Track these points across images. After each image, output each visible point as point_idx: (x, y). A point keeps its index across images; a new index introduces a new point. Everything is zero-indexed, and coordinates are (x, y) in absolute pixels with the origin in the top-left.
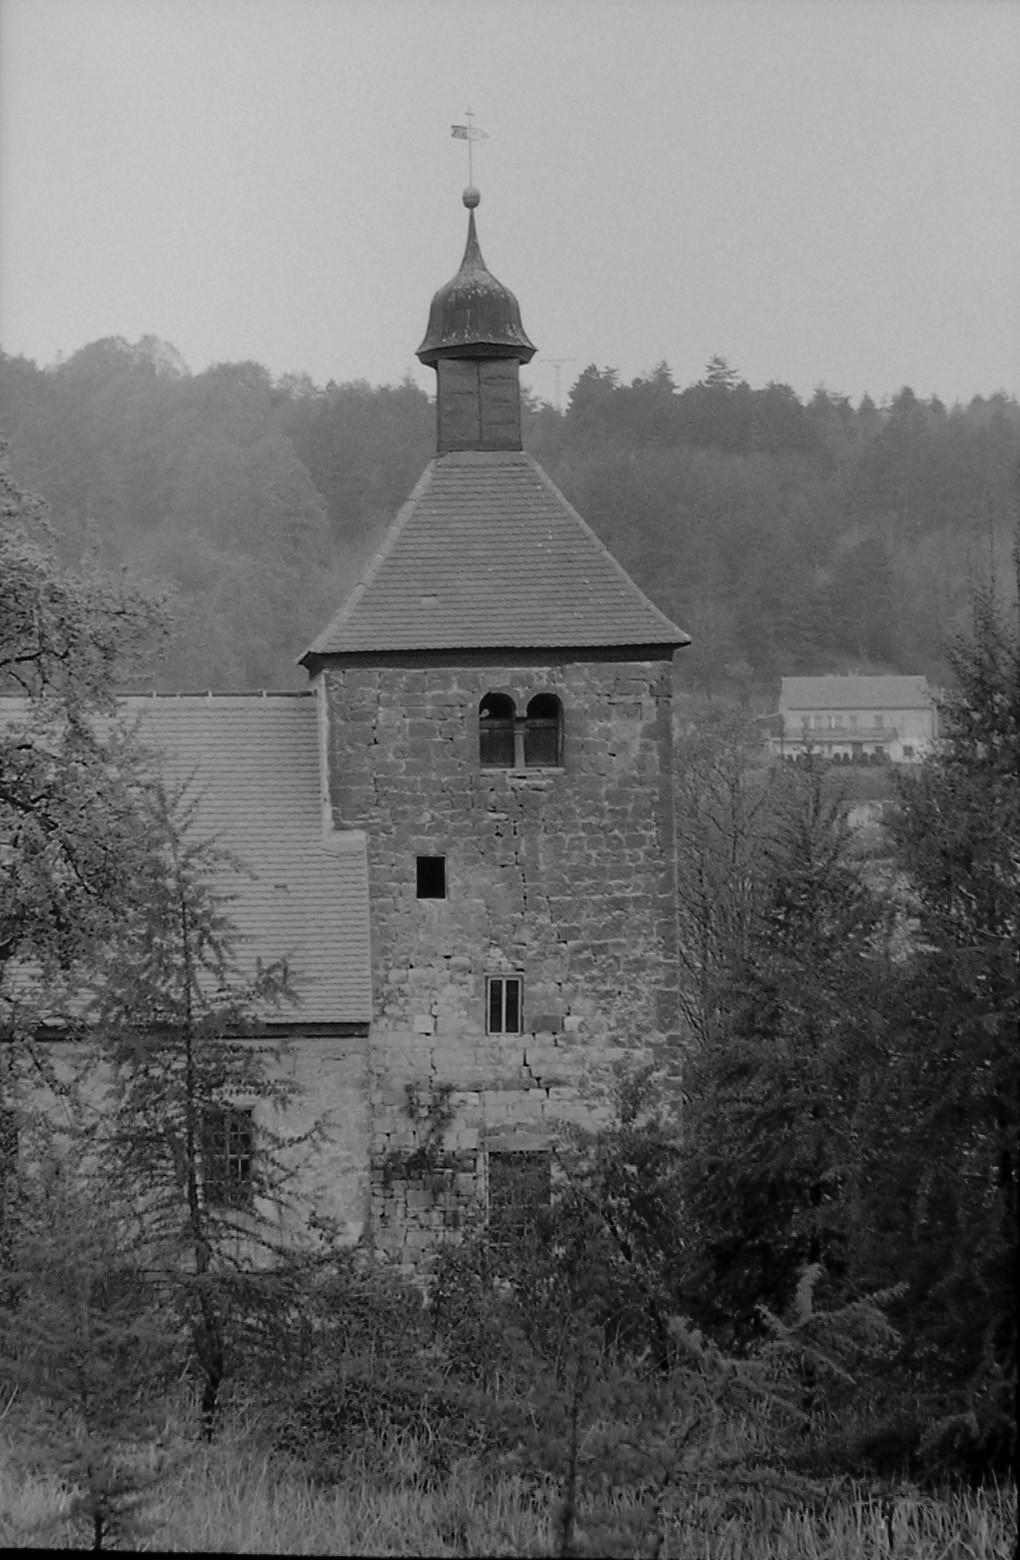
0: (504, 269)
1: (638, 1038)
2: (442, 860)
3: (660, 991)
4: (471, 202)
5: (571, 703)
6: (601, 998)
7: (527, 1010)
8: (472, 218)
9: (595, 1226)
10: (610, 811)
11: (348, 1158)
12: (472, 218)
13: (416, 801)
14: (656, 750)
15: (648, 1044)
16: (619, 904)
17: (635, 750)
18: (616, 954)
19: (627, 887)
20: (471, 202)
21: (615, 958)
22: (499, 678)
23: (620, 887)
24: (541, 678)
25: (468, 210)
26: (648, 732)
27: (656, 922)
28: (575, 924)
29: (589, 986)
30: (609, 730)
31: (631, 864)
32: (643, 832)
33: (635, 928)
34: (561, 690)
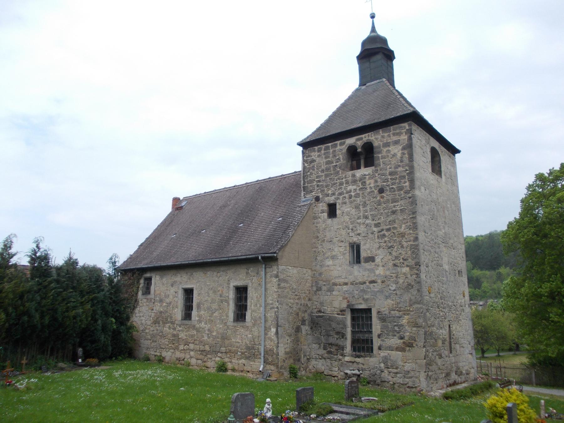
0: (381, 32)
1: (403, 263)
2: (336, 205)
3: (411, 245)
4: (373, 17)
5: (376, 144)
6: (389, 249)
7: (363, 254)
8: (373, 21)
9: (36, 248)
10: (391, 179)
11: (272, 304)
12: (373, 21)
13: (327, 186)
14: (407, 154)
15: (407, 266)
16: (394, 212)
17: (399, 155)
18: (394, 231)
19: (397, 206)
20: (373, 17)
21: (393, 232)
22: (350, 141)
23: (394, 206)
24: (366, 137)
25: (371, 20)
26: (404, 149)
27: (409, 218)
28: (379, 221)
29: (385, 244)
30: (389, 150)
31: (398, 197)
32: (403, 185)
33: (401, 221)
34: (373, 140)
